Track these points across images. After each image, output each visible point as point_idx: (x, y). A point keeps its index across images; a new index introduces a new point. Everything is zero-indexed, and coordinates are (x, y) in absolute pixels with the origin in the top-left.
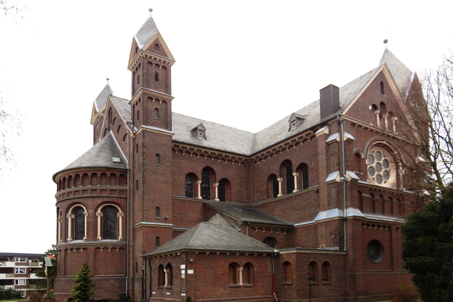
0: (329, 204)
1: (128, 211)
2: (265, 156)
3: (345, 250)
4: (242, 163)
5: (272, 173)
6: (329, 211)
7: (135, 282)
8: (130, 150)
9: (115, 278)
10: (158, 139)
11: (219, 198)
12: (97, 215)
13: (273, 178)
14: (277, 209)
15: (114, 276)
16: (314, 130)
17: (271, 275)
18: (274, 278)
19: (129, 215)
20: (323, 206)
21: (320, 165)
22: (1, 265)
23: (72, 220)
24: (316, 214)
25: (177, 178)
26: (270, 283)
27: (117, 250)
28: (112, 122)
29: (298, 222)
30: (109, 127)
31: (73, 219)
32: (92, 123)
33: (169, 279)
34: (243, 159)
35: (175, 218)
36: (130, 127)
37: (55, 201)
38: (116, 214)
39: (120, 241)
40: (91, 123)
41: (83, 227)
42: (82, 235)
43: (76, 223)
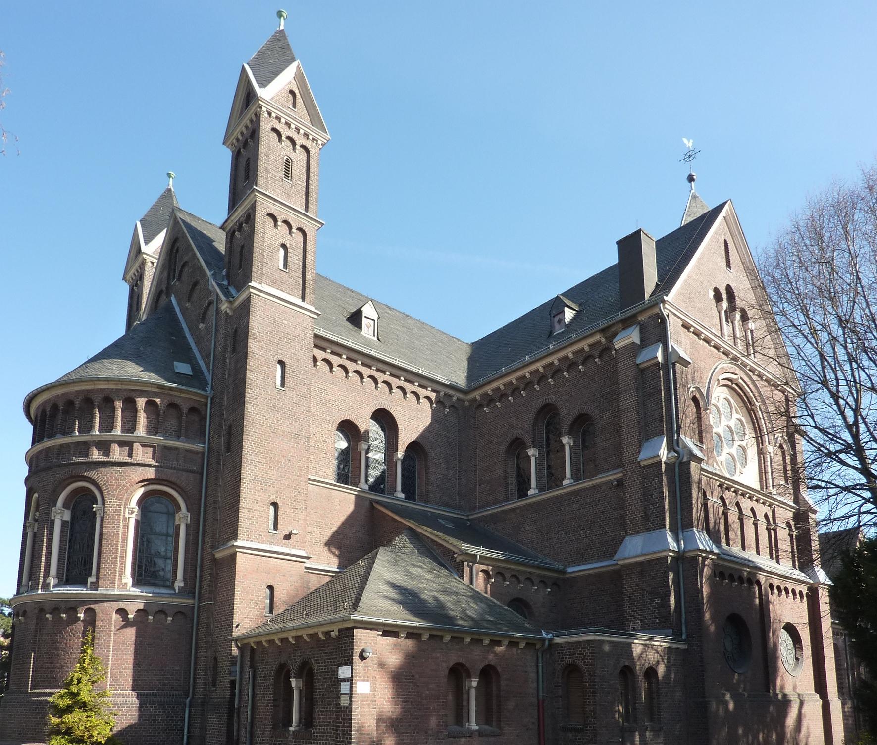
0: (647, 518)
1: (202, 509)
2: (500, 393)
3: (684, 637)
4: (452, 406)
6: (647, 535)
7: (210, 715)
8: (218, 344)
9: (158, 699)
10: (284, 322)
11: (403, 491)
13: (517, 447)
14: (528, 528)
15: (155, 695)
16: (608, 335)
17: (535, 701)
18: (541, 710)
19: (631, 309)
20: (632, 521)
23: (64, 523)
25: (318, 429)
26: (533, 723)
27: (169, 618)
28: (177, 275)
29: (575, 563)
30: (167, 288)
32: (128, 277)
33: (303, 709)
34: (455, 398)
35: (308, 537)
36: (219, 285)
37: (25, 470)
38: (174, 515)
39: (177, 592)
40: (124, 279)
41: (88, 546)
42: (86, 570)
43: (71, 535)
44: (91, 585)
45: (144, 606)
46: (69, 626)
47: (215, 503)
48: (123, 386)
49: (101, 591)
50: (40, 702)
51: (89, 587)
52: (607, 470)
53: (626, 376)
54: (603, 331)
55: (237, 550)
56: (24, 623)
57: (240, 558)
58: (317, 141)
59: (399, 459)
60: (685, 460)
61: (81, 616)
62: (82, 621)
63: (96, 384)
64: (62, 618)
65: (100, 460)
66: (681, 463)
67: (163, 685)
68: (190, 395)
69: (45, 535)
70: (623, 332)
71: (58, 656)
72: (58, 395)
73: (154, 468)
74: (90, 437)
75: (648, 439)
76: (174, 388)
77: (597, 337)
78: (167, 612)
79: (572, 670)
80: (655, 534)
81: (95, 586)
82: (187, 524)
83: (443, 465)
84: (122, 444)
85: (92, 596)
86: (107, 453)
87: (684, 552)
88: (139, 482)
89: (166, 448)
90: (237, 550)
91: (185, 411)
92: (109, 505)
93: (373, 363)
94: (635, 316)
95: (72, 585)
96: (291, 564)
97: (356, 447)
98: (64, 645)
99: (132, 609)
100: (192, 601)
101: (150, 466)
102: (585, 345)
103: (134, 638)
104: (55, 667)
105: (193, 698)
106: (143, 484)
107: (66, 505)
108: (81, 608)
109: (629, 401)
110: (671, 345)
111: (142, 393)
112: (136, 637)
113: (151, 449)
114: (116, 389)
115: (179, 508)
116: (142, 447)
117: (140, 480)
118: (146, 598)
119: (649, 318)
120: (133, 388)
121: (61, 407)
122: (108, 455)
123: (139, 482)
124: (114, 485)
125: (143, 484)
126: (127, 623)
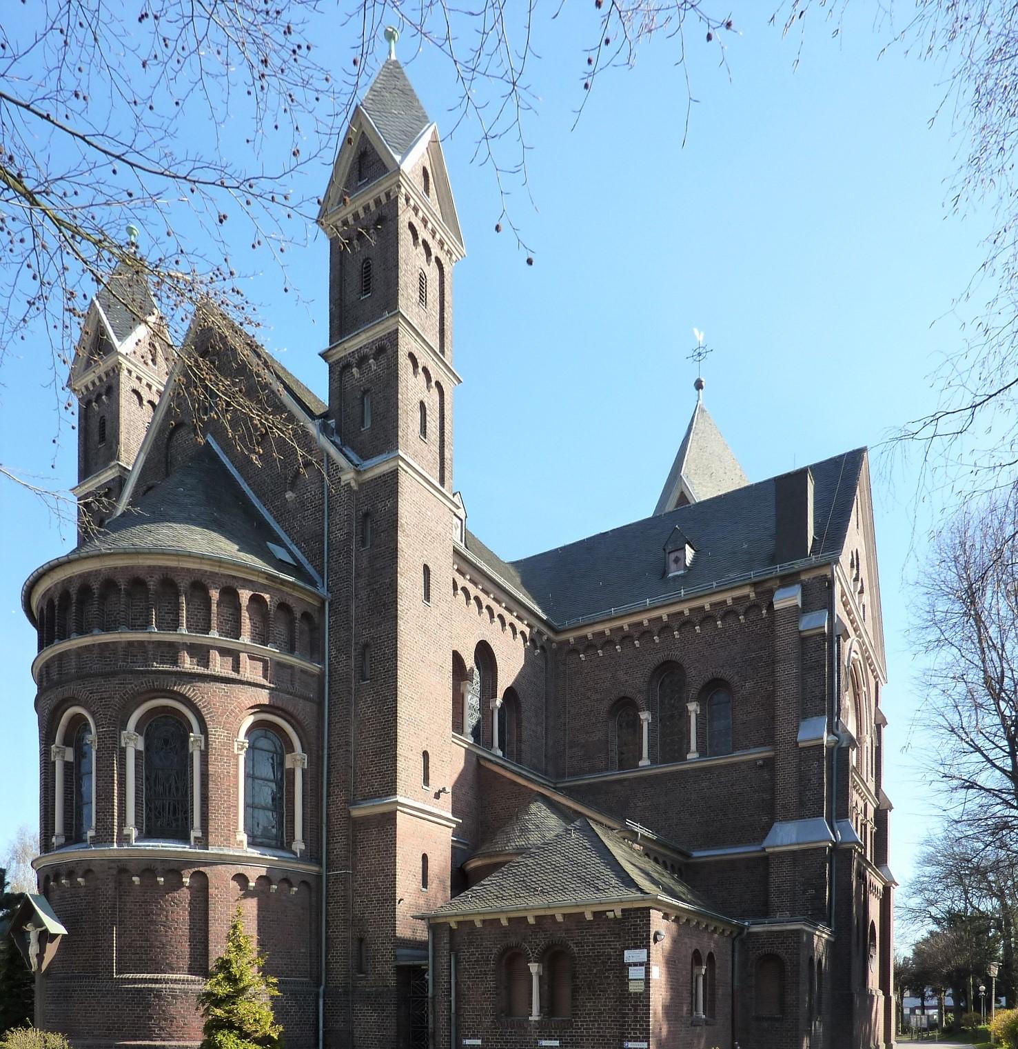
0: (802, 804)
5: (622, 694)
6: (801, 823)
12: (236, 752)
13: (625, 708)
21: (780, 693)
22: (1016, 818)
23: (138, 753)
24: (766, 830)
29: (701, 847)
31: (140, 752)
39: (298, 856)
44: (195, 842)
45: (267, 871)
46: (167, 893)
47: (347, 745)
48: (222, 569)
49: (212, 850)
50: (140, 990)
51: (192, 844)
52: (747, 748)
53: (785, 642)
54: (755, 585)
55: (399, 808)
56: (85, 886)
57: (400, 817)
58: (451, 255)
59: (496, 707)
60: (844, 745)
61: (186, 880)
62: (188, 887)
63: (204, 564)
64: (158, 882)
65: (193, 671)
66: (840, 749)
67: (290, 971)
68: (302, 598)
69: (115, 768)
70: (781, 590)
71: (156, 932)
72: (116, 568)
73: (268, 691)
74: (180, 637)
75: (806, 718)
76: (289, 582)
77: (746, 591)
78: (292, 880)
79: (771, 958)
80: (811, 822)
81: (204, 842)
82: (302, 770)
83: (533, 720)
84: (224, 652)
85: (202, 856)
86: (205, 662)
87: (841, 843)
88: (251, 708)
89: (280, 665)
90: (399, 808)
91: (298, 615)
92: (215, 735)
93: (481, 580)
94: (798, 573)
95: (167, 840)
96: (440, 829)
97: (458, 687)
98: (164, 919)
99: (254, 873)
100: (316, 869)
101: (263, 687)
102: (728, 597)
103: (256, 912)
104: (152, 946)
105: (326, 986)
106: (253, 711)
107: (138, 728)
108: (186, 871)
109: (787, 672)
110: (837, 616)
111: (247, 583)
112: (258, 910)
113: (261, 664)
114: (211, 572)
115: (291, 749)
116: (250, 659)
117: (251, 705)
118: (271, 862)
119: (814, 578)
120: (234, 573)
121: (123, 587)
122: (207, 666)
123: (251, 708)
124: (218, 709)
125: (253, 711)
126: (248, 893)
